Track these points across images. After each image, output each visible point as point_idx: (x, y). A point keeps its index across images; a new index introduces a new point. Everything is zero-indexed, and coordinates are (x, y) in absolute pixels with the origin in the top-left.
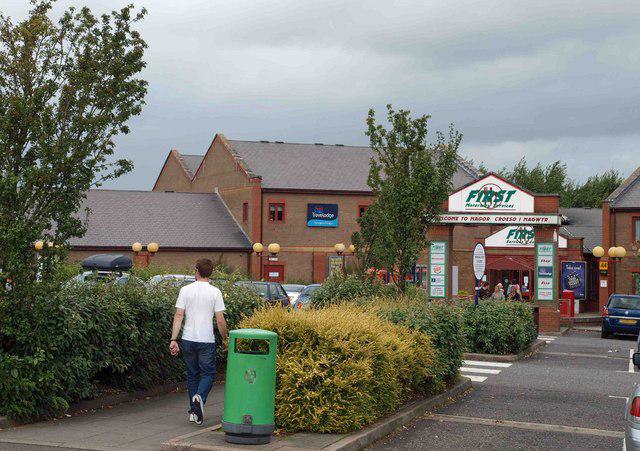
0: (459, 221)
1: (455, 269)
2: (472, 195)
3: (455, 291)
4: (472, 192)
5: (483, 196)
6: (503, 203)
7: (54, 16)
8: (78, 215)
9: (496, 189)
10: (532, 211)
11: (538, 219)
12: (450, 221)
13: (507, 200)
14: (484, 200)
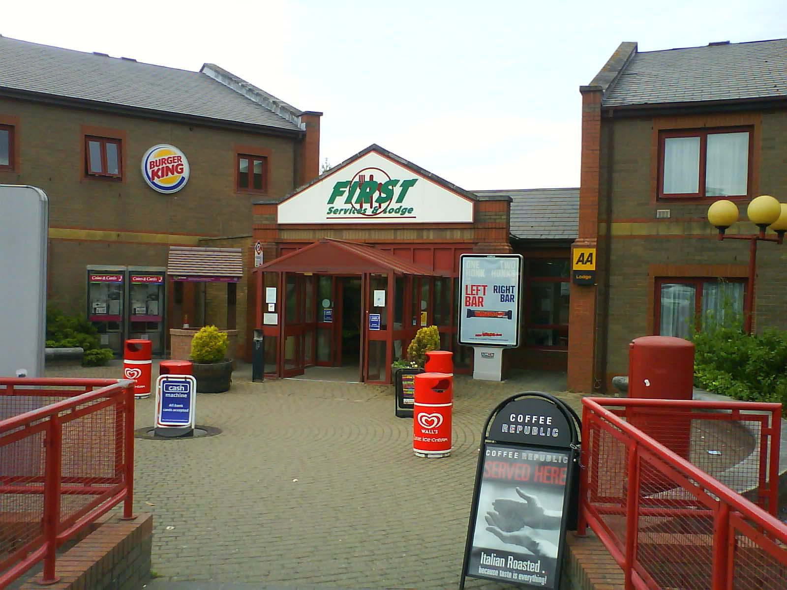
1: (498, 316)
6: (394, 205)
7: (420, 556)
8: (240, 376)
9: (380, 179)
13: (400, 200)
14: (360, 201)
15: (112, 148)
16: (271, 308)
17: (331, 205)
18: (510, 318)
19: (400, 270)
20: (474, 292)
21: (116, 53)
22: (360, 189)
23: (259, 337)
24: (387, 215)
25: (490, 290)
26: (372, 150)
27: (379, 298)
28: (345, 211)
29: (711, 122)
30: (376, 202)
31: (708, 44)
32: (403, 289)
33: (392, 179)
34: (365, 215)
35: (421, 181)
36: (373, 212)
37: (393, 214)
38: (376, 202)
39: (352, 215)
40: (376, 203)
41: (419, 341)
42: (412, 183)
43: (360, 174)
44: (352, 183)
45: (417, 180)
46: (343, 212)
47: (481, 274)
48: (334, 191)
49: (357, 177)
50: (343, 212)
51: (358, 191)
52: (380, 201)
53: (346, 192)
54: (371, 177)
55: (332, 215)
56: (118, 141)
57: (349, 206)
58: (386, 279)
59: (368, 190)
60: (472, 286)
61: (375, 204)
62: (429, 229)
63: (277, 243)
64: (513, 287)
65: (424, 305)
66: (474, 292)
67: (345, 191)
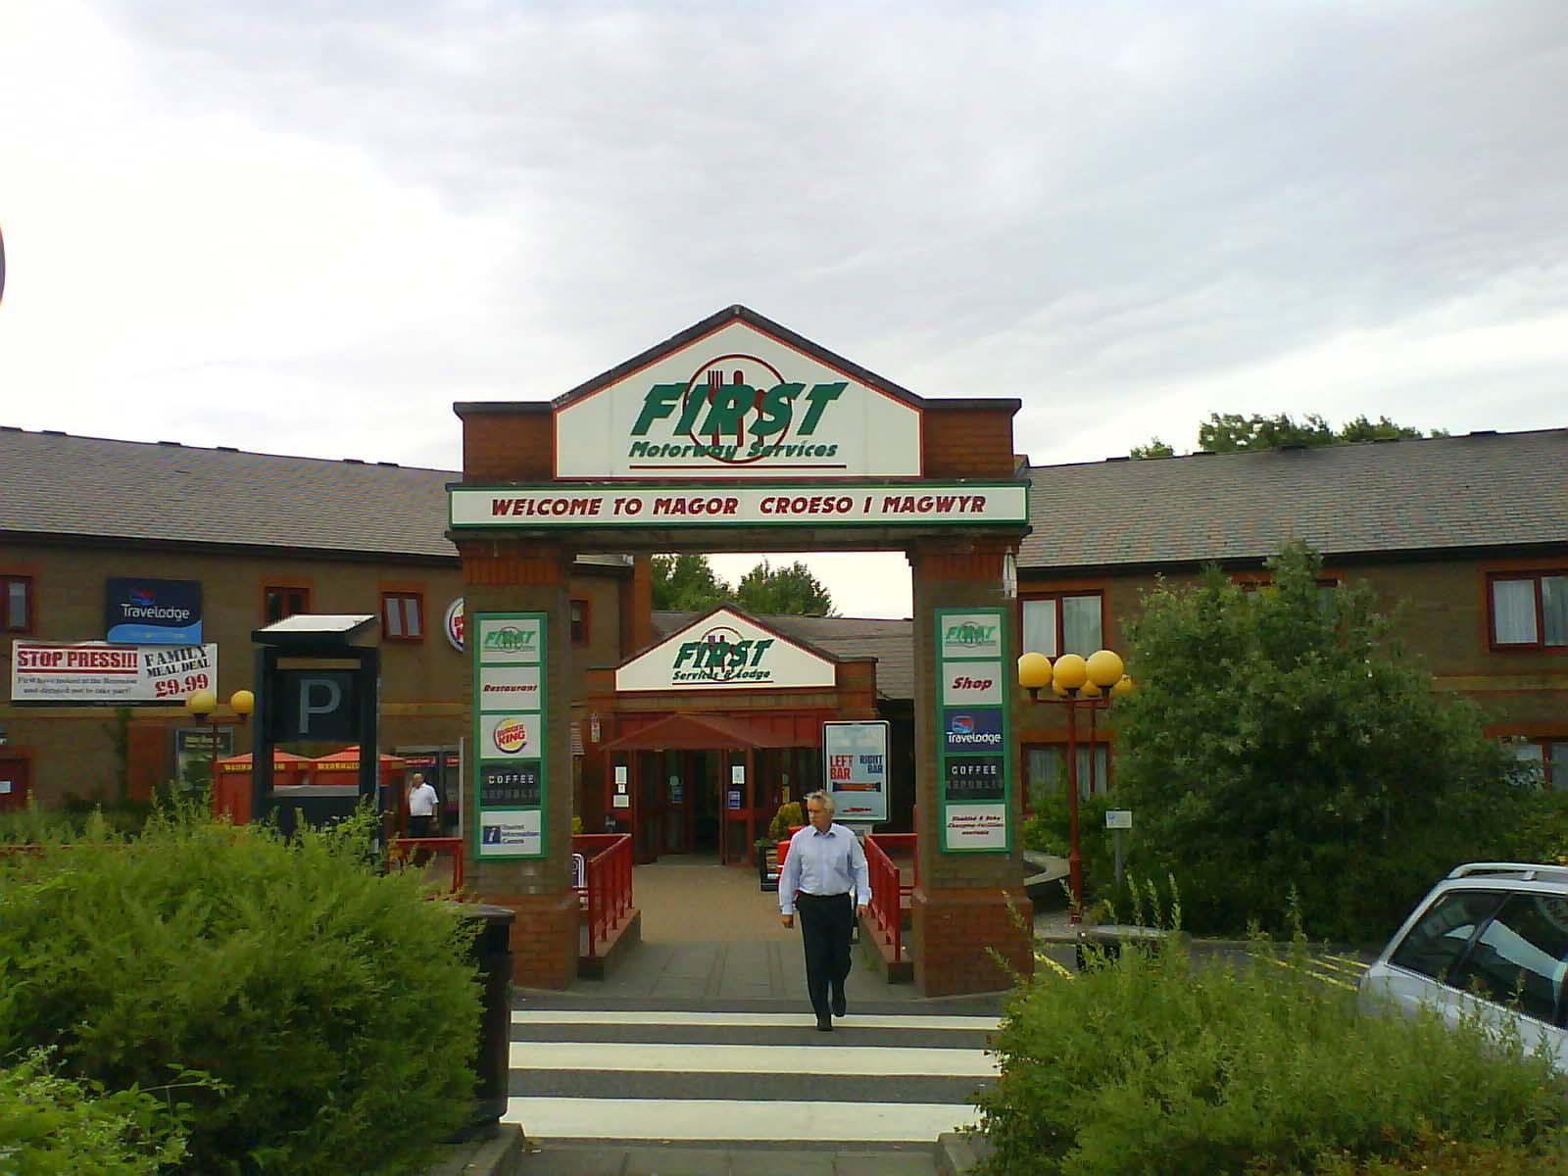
0: (606, 515)
2: (684, 654)
3: (992, 1024)
4: (686, 647)
5: (706, 407)
6: (748, 668)
10: (915, 470)
11: (945, 504)
12: (565, 519)
13: (808, 427)
15: (411, 604)
16: (622, 789)
17: (677, 670)
18: (879, 790)
19: (759, 744)
20: (840, 763)
21: (371, 457)
22: (711, 403)
23: (610, 820)
24: (741, 679)
25: (856, 761)
26: (723, 607)
27: (738, 775)
28: (695, 677)
29: (1066, 586)
30: (749, 431)
31: (1105, 460)
32: (762, 764)
33: (787, 382)
34: (732, 462)
35: (854, 386)
36: (725, 676)
37: (748, 679)
38: (749, 431)
39: (701, 680)
40: (750, 435)
41: (782, 819)
42: (836, 391)
43: (711, 368)
44: (692, 388)
45: (772, 641)
46: (691, 677)
47: (846, 742)
48: (647, 404)
49: (704, 375)
50: (691, 677)
51: (708, 653)
52: (733, 663)
53: (676, 410)
54: (722, 637)
55: (679, 681)
56: (418, 596)
57: (684, 441)
58: (744, 753)
59: (731, 405)
60: (837, 757)
61: (727, 668)
62: (788, 694)
63: (616, 713)
64: (881, 756)
65: (785, 778)
66: (840, 763)
67: (674, 406)
